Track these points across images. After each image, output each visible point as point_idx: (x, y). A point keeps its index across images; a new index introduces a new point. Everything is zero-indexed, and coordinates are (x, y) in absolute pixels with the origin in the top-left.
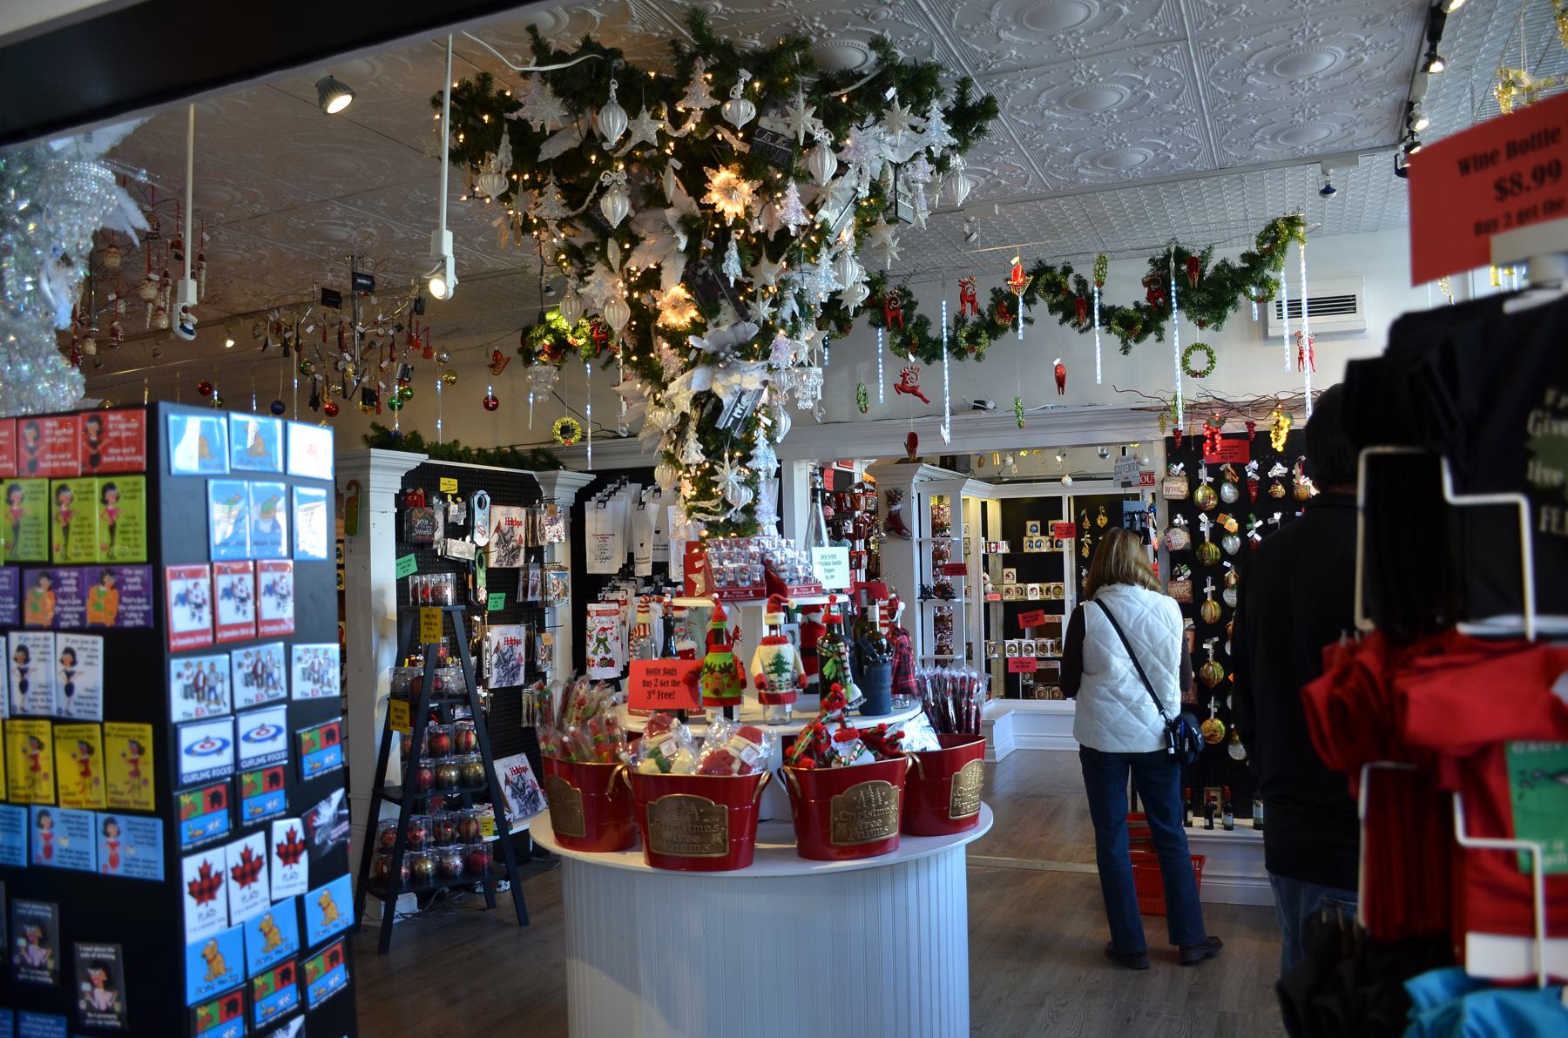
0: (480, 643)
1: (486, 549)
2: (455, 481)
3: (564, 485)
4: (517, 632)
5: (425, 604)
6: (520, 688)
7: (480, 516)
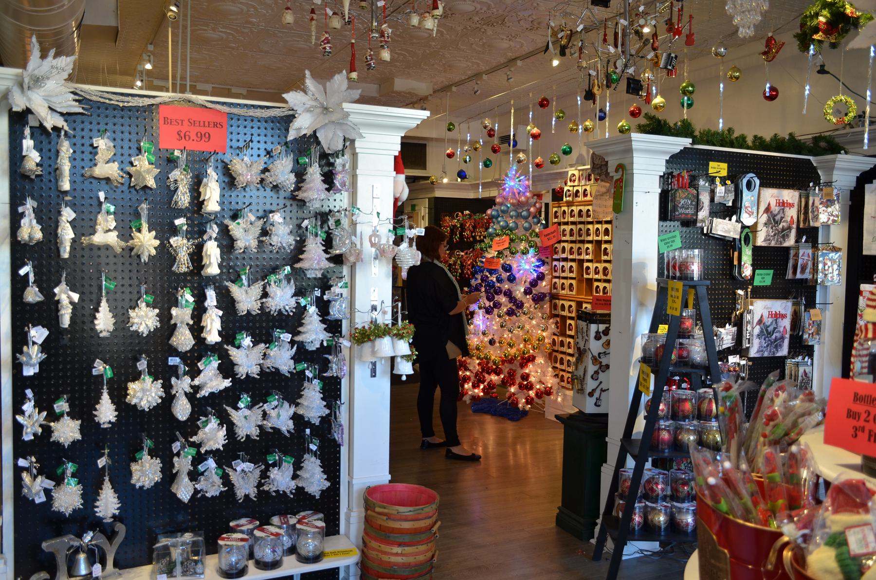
0: (742, 314)
1: (754, 229)
2: (724, 166)
3: (843, 171)
4: (783, 306)
5: (674, 278)
6: (783, 359)
7: (748, 198)
